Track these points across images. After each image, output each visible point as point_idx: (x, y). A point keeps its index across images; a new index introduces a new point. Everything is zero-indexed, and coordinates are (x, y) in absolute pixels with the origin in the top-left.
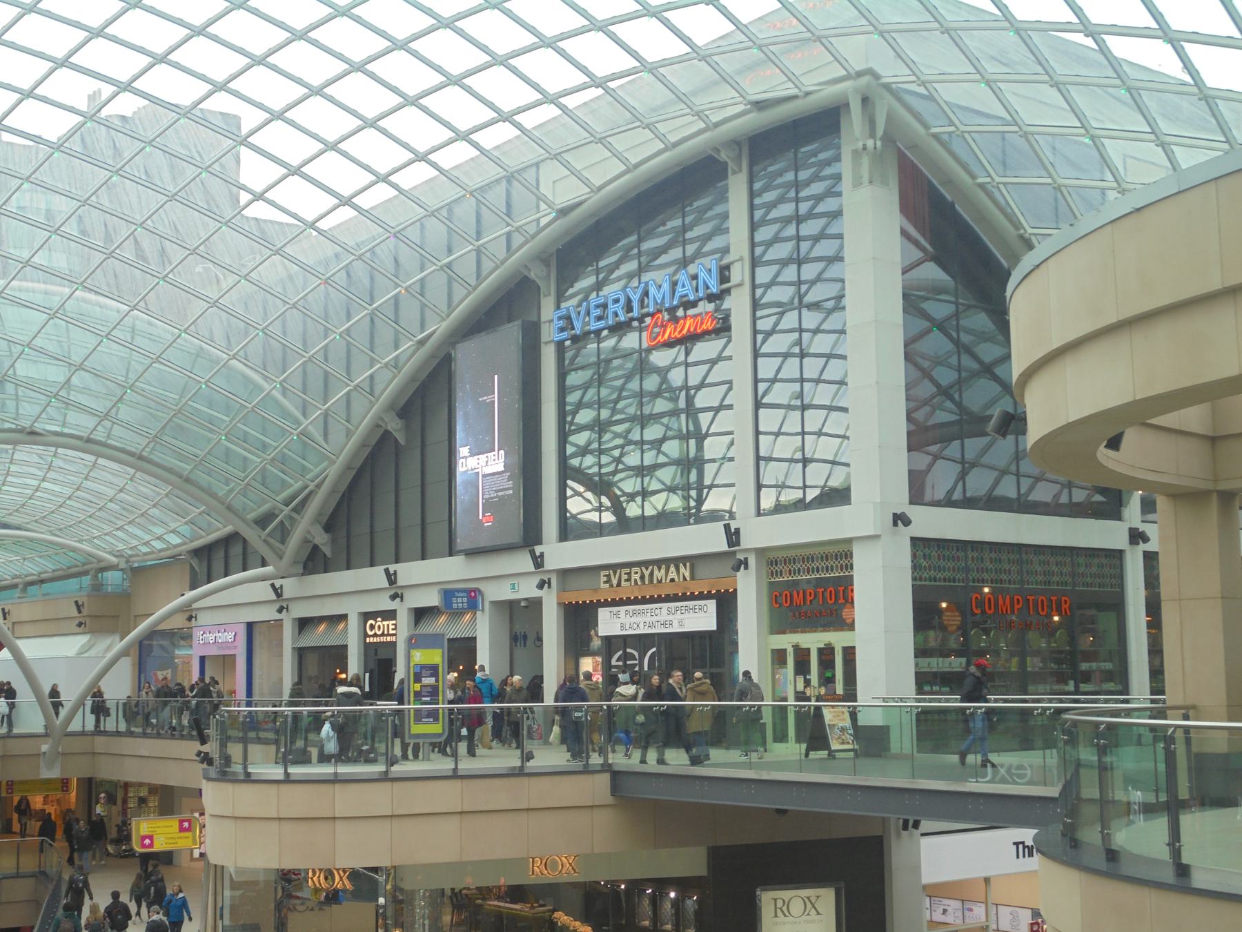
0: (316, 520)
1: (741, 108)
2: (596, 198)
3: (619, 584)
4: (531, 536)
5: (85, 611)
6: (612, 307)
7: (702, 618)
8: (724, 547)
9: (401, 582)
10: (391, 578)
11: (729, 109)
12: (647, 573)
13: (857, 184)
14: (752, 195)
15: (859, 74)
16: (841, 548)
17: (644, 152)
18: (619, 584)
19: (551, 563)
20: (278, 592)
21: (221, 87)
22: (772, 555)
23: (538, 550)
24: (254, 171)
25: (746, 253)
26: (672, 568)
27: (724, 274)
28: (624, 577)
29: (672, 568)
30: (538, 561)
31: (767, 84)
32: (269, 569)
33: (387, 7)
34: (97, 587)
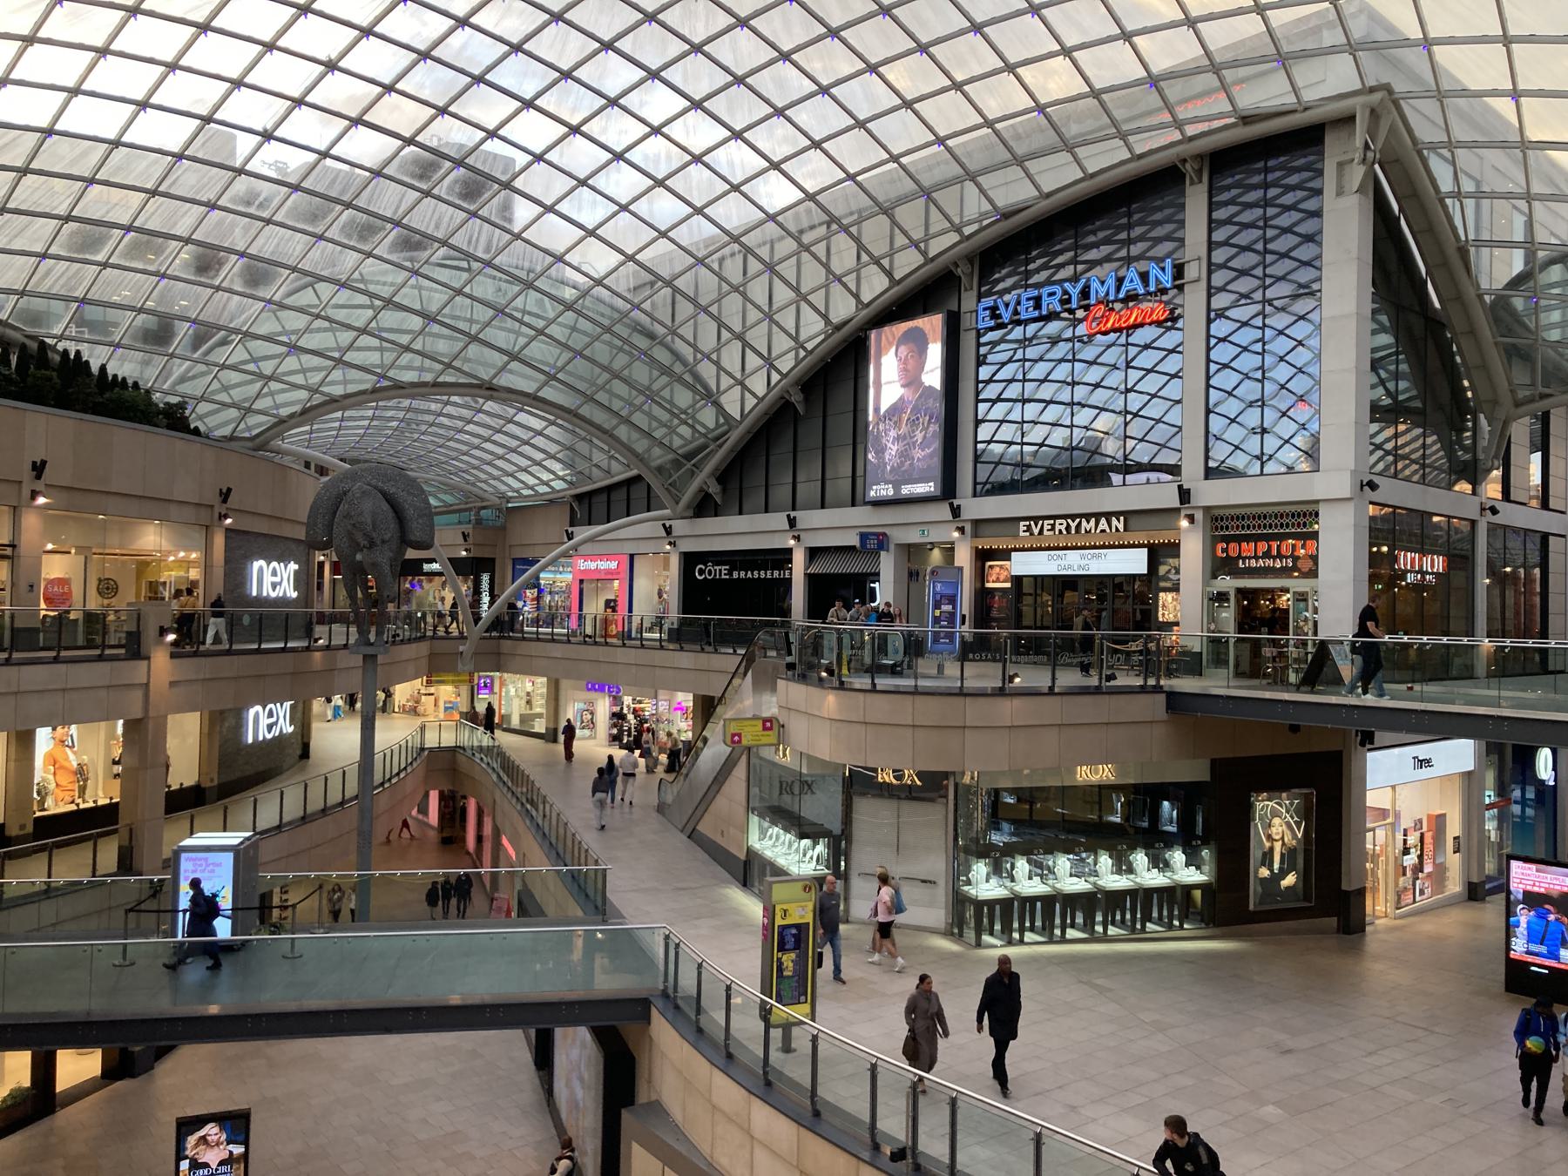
0: (712, 474)
1: (1233, 120)
2: (1045, 204)
3: (1041, 532)
4: (948, 490)
5: (470, 540)
6: (1045, 301)
7: (1132, 562)
8: (1177, 504)
9: (800, 525)
10: (792, 522)
11: (1209, 115)
12: (1074, 525)
13: (1340, 192)
14: (1212, 206)
15: (1372, 90)
16: (1310, 508)
17: (1106, 158)
18: (1041, 532)
19: (967, 514)
20: (668, 530)
21: (492, 134)
22: (1216, 512)
23: (956, 502)
24: (156, 397)
25: (1203, 251)
26: (1103, 520)
27: (1179, 271)
28: (1046, 527)
29: (1103, 520)
30: (956, 512)
31: (1267, 93)
32: (667, 512)
33: (930, 15)
34: (479, 522)
